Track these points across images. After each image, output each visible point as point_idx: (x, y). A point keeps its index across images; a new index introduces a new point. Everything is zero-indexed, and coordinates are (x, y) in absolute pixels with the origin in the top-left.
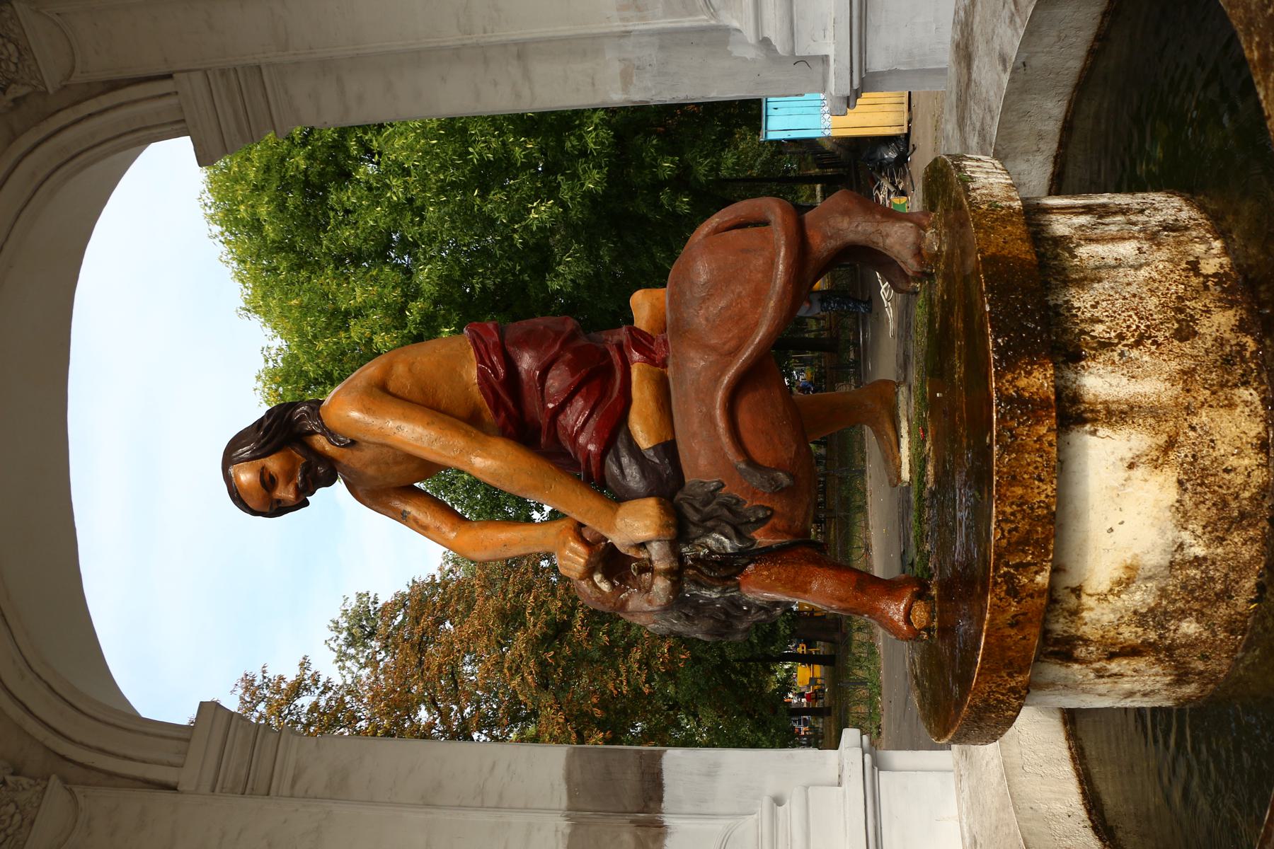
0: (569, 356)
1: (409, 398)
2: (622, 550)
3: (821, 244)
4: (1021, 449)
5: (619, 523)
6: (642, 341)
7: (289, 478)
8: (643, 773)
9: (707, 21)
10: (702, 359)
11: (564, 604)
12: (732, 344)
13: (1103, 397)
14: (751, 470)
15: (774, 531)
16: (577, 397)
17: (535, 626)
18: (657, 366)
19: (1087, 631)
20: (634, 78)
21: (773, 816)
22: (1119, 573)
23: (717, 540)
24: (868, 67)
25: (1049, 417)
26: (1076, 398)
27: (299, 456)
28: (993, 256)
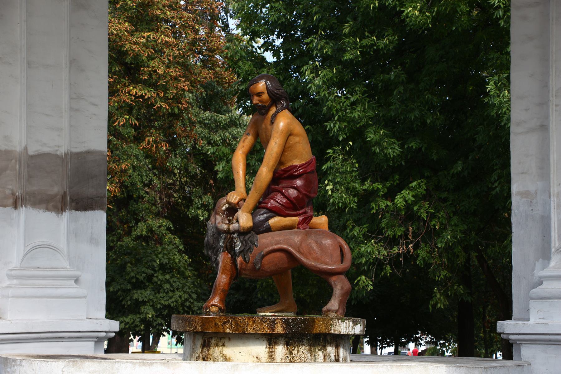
0: (301, 196)
1: (287, 143)
2: (236, 214)
3: (333, 280)
4: (262, 324)
5: (245, 214)
6: (307, 220)
7: (261, 101)
8: (92, 198)
9: (554, 247)
10: (298, 241)
11: (160, 77)
12: (302, 251)
13: (276, 351)
14: (261, 256)
15: (241, 263)
16: (286, 200)
17: (136, 43)
18: (298, 225)
19: (212, 349)
20: (525, 199)
21: (69, 278)
22: (228, 356)
23: (239, 245)
24: (523, 345)
25: (270, 331)
26: (276, 343)
27: (268, 104)
28: (314, 322)
